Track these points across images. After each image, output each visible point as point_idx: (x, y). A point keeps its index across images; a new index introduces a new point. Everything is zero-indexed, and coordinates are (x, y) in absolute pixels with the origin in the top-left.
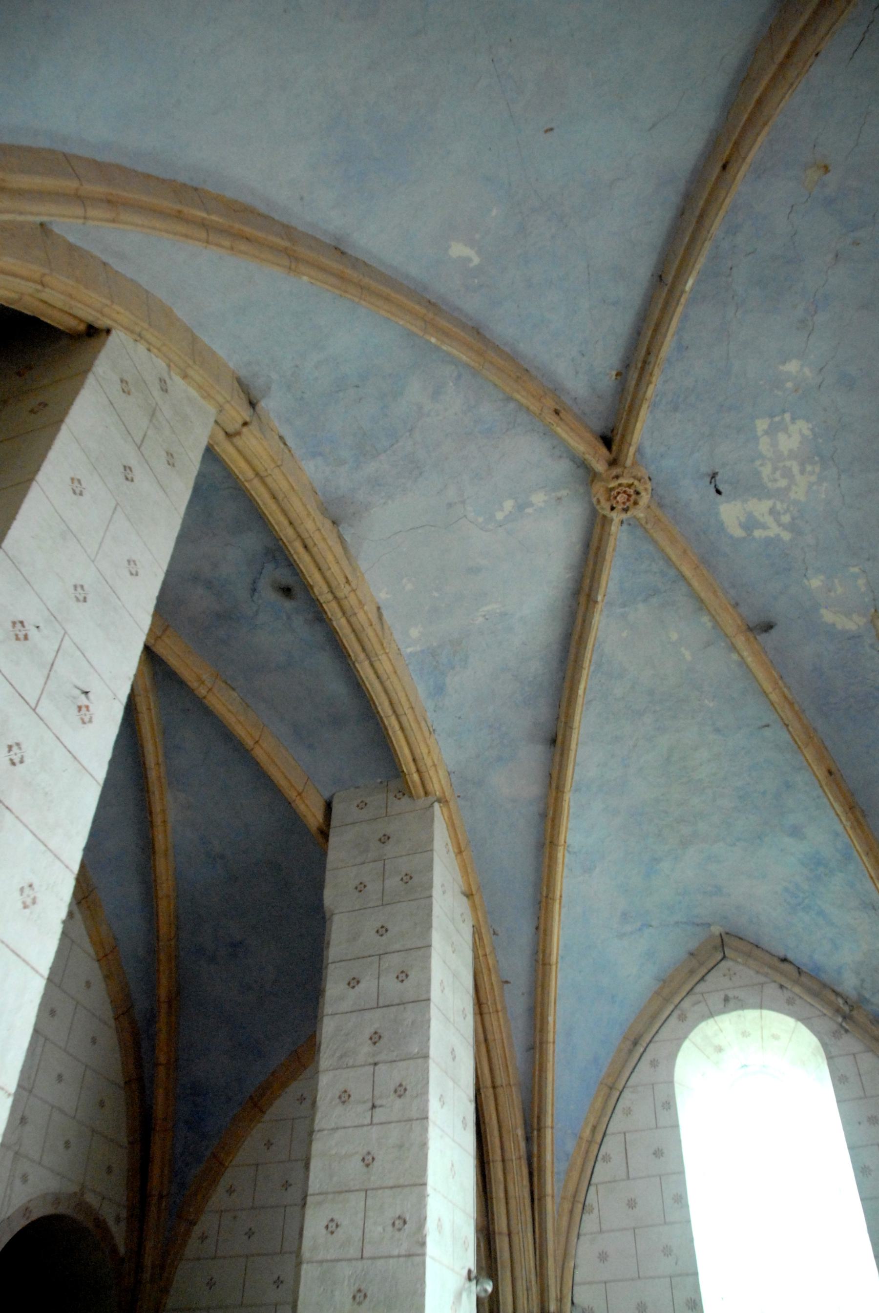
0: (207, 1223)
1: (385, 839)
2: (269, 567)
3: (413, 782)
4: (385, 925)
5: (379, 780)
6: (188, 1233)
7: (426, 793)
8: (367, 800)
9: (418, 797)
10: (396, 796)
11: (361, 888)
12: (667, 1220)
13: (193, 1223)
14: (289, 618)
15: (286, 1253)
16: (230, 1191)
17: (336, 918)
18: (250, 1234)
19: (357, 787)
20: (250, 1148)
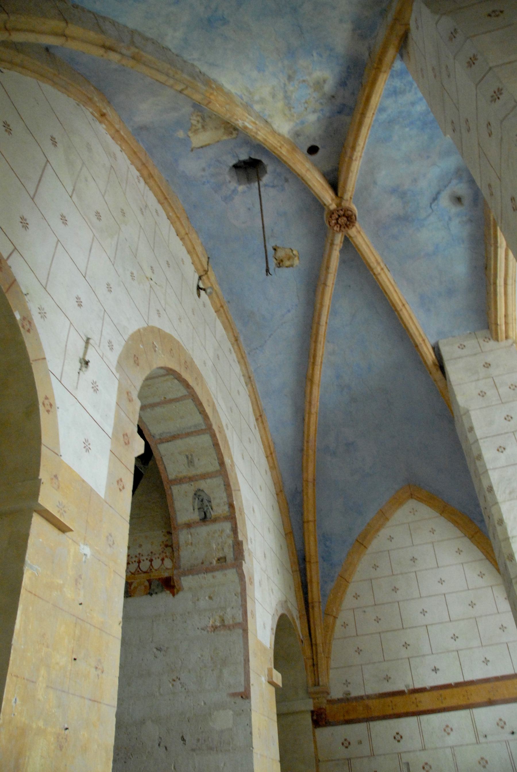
0: (344, 615)
1: (487, 365)
2: (454, 182)
3: (501, 330)
4: (509, 414)
5: (468, 332)
6: (334, 623)
7: (507, 338)
8: (465, 344)
9: (502, 341)
10: (484, 341)
11: (482, 394)
12: (404, 626)
13: (335, 618)
14: (450, 219)
15: (406, 628)
16: (356, 596)
17: (472, 413)
18: (378, 620)
19: (454, 337)
20: (363, 568)
